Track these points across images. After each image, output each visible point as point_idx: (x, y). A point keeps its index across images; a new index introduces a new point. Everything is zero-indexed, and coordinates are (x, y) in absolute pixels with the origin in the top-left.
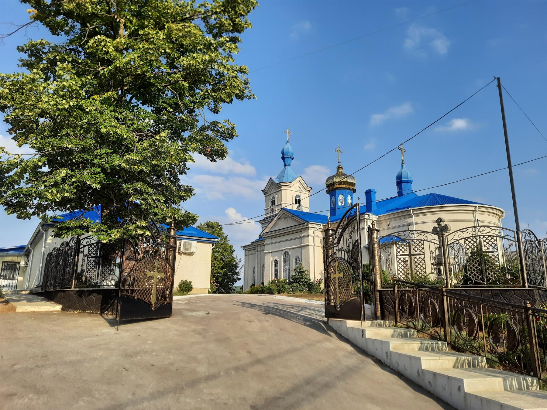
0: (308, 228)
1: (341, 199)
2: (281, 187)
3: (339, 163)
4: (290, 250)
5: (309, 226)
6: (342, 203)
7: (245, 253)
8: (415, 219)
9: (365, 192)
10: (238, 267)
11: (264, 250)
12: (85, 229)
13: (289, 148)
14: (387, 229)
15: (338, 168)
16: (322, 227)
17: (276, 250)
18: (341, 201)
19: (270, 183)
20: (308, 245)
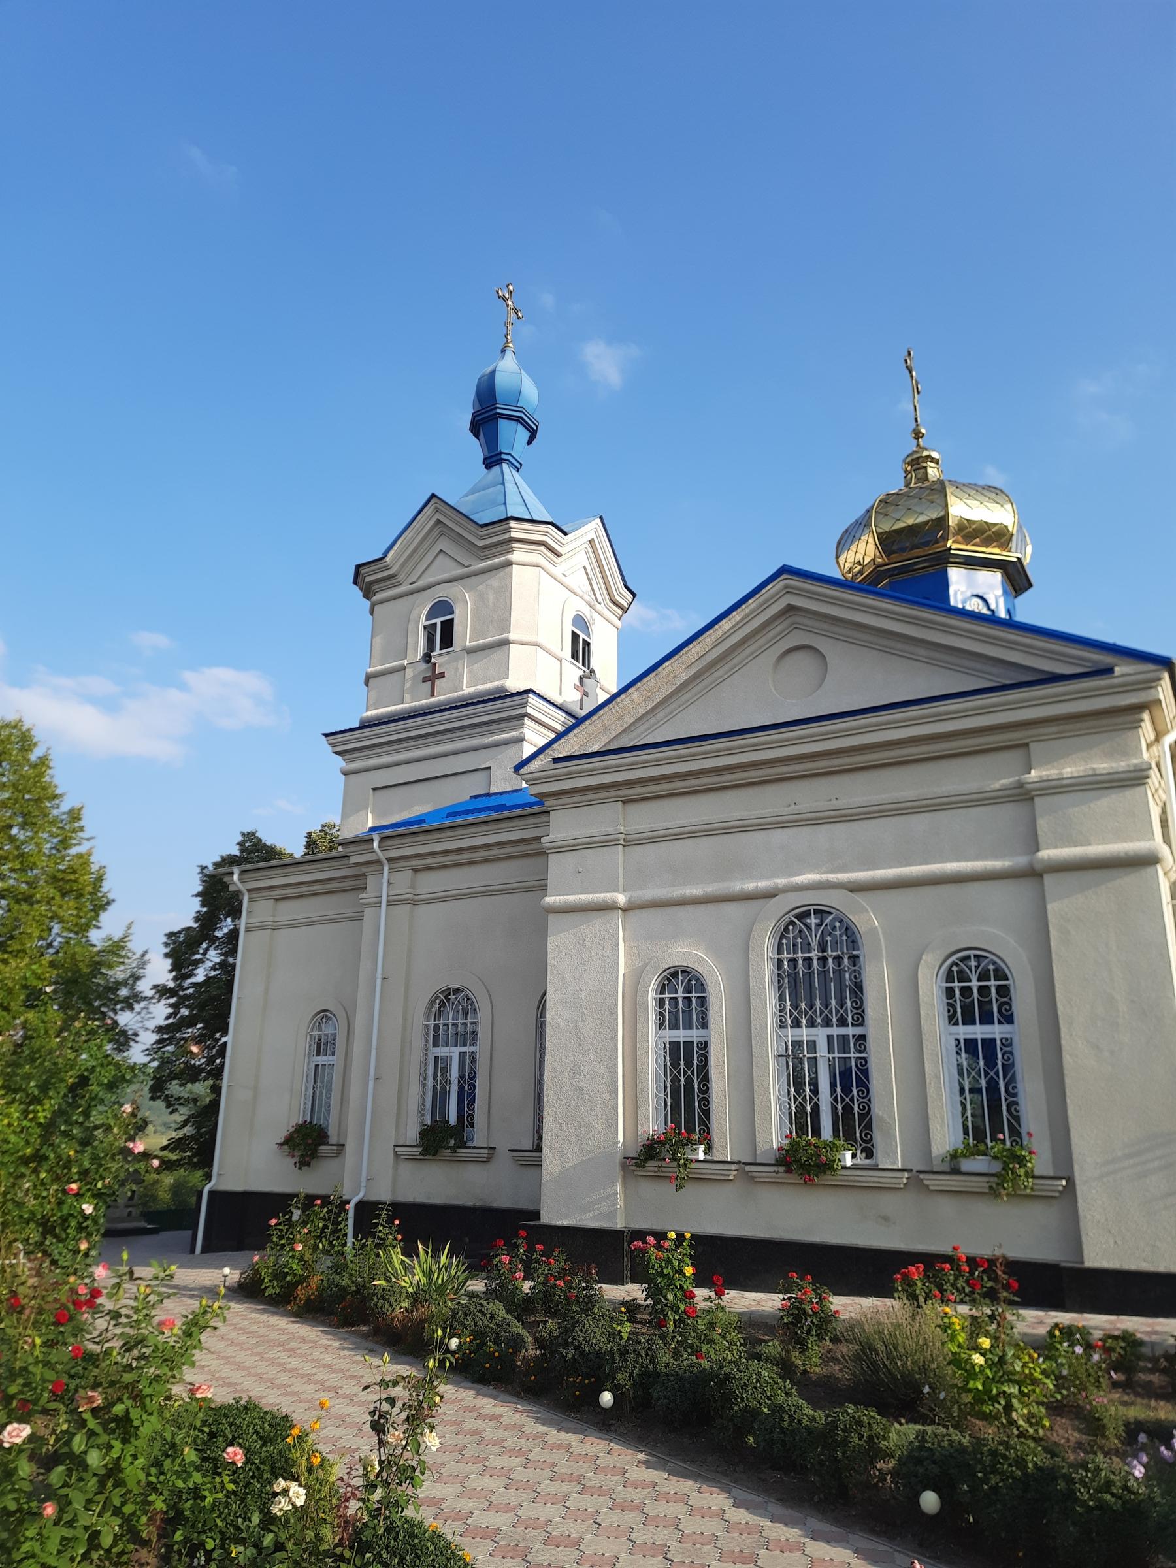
2: (507, 544)
13: (508, 369)
20: (1150, 860)
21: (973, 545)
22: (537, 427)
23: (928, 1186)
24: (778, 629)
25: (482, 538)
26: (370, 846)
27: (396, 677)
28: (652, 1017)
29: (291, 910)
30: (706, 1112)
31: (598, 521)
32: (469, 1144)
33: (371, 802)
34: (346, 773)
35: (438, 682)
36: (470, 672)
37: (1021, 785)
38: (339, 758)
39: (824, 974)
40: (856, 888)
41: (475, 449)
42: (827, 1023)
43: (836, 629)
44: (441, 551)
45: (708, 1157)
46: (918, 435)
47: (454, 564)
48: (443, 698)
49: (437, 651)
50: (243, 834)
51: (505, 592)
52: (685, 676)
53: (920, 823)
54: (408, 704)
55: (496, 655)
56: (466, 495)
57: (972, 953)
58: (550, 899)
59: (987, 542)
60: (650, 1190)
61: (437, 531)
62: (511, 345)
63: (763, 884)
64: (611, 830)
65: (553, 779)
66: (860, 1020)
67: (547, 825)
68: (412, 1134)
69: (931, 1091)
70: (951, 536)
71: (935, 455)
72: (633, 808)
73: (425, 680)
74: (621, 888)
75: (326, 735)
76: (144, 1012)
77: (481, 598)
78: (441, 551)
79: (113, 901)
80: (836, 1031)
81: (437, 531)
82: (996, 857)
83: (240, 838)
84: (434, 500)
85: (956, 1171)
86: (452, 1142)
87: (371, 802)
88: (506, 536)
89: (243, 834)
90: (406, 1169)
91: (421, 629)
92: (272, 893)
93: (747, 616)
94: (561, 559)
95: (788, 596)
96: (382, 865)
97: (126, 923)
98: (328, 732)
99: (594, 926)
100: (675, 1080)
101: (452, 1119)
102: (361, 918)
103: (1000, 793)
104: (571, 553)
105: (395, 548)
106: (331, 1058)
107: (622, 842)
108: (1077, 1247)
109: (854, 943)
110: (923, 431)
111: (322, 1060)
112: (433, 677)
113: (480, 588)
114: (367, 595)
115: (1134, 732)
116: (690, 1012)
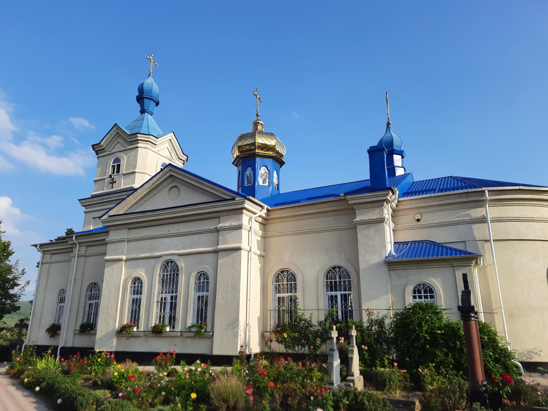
0: (239, 211)
1: (263, 175)
2: (137, 141)
3: (257, 115)
4: (180, 258)
5: (246, 206)
6: (264, 181)
7: (43, 258)
8: (491, 212)
9: (369, 151)
10: (17, 285)
11: (105, 254)
12: (316, 356)
13: (150, 83)
14: (412, 228)
15: (256, 124)
16: (263, 213)
17: (147, 255)
18: (264, 177)
19: (114, 132)
20: (239, 249)
21: (264, 151)
22: (158, 101)
23: (184, 336)
24: (170, 180)
25: (130, 139)
26: (72, 239)
27: (102, 182)
28: (129, 291)
29: (55, 258)
30: (139, 318)
31: (172, 133)
32: (94, 329)
33: (92, 223)
34: (85, 213)
35: (114, 184)
36: (124, 181)
37: (217, 228)
38: (83, 207)
39: (170, 279)
40: (180, 255)
41: (138, 107)
42: (169, 293)
43: (182, 182)
44: (118, 142)
45: (138, 330)
46: (257, 115)
47: (121, 146)
48: (115, 189)
49: (115, 174)
50: (68, 230)
51: (136, 156)
52: (145, 193)
53: (196, 237)
54: (106, 191)
55: (132, 176)
56: (132, 123)
57: (202, 273)
58: (107, 257)
59: (268, 150)
60: (123, 340)
61: (117, 135)
62: (151, 74)
63: (159, 254)
64: (123, 237)
65: (109, 222)
66: (176, 292)
67: (108, 235)
68: (78, 328)
69: (188, 311)
70: (256, 148)
71: (261, 122)
72: (131, 231)
73: (110, 183)
74: (125, 253)
75: (79, 200)
76: (22, 289)
77: (129, 158)
78: (118, 142)
79: (14, 252)
80: (343, 293)
81: (117, 135)
82: (211, 247)
83: (66, 231)
84: (116, 126)
85: (190, 332)
86: (89, 329)
87: (92, 223)
88: (136, 139)
89: (68, 230)
90: (77, 337)
91: (111, 167)
92: (50, 252)
93: (160, 177)
94: (156, 146)
95: (171, 172)
96: (77, 245)
97: (16, 260)
98: (79, 199)
99: (117, 265)
100: (132, 309)
101: (91, 322)
102: (71, 261)
103: (213, 230)
104: (160, 144)
105: (104, 140)
106: (64, 304)
107: (126, 241)
108: (212, 349)
109: (178, 270)
110: (259, 114)
111: (61, 304)
112: (113, 182)
113: (128, 154)
114: (97, 154)
115: (242, 215)
116: (341, 286)
